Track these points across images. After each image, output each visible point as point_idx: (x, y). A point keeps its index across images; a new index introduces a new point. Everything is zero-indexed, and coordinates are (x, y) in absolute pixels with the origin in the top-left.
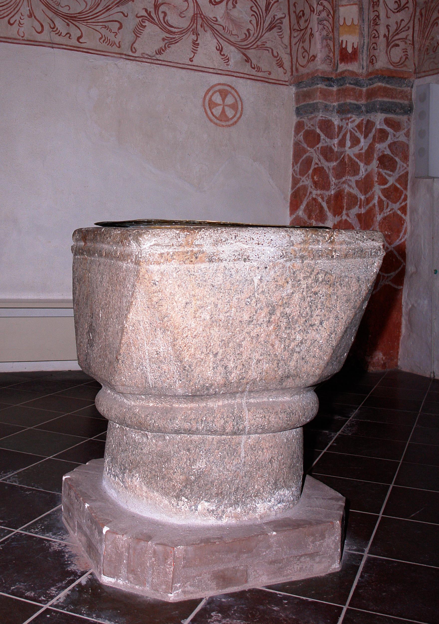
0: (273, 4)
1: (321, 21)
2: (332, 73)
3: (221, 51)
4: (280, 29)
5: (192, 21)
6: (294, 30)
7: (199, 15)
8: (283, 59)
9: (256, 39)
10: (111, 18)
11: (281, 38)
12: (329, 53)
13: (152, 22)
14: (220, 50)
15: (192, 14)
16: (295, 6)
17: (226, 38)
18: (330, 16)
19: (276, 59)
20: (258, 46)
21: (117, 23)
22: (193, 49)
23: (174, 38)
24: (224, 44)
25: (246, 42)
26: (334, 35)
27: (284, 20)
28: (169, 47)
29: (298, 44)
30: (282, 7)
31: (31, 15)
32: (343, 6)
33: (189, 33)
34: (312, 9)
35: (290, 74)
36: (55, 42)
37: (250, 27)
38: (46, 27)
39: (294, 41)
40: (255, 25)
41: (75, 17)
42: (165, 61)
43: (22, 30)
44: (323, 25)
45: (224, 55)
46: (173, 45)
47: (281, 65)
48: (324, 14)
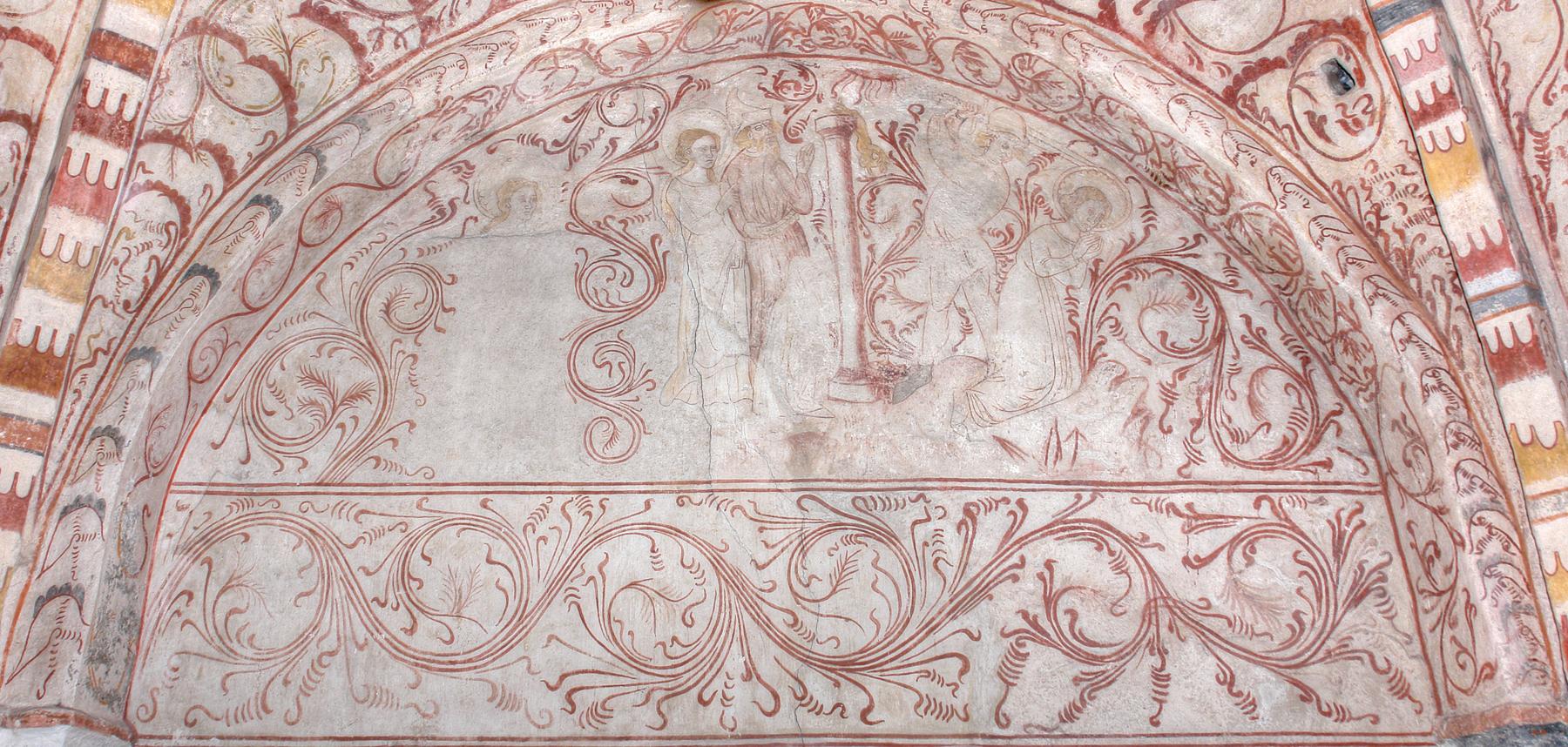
0: (1352, 536)
1: (1489, 567)
2: (1555, 711)
3: (1231, 684)
4: (1384, 595)
5: (1144, 620)
6: (1421, 592)
7: (1160, 602)
8: (1406, 674)
9: (1320, 634)
10: (939, 650)
11: (1391, 618)
12: (1535, 651)
13: (1042, 642)
14: (1228, 681)
15: (1144, 602)
16: (1411, 532)
17: (1240, 648)
18: (1513, 549)
19: (1385, 678)
20: (1329, 653)
21: (955, 659)
22: (1156, 692)
23: (1104, 672)
24: (1237, 664)
25: (1294, 647)
26: (1535, 598)
27: (1389, 571)
28: (1091, 698)
29: (1438, 629)
30: (1376, 536)
31: (750, 674)
32: (1542, 520)
33: (1140, 654)
34: (1458, 539)
35: (1433, 711)
36: (808, 732)
37: (1301, 604)
38: (786, 698)
39: (1427, 621)
40: (1313, 599)
41: (853, 663)
42: (1086, 736)
43: (730, 712)
44: (1496, 576)
45: (1239, 694)
46: (1103, 691)
47: (1401, 690)
48: (1494, 548)
